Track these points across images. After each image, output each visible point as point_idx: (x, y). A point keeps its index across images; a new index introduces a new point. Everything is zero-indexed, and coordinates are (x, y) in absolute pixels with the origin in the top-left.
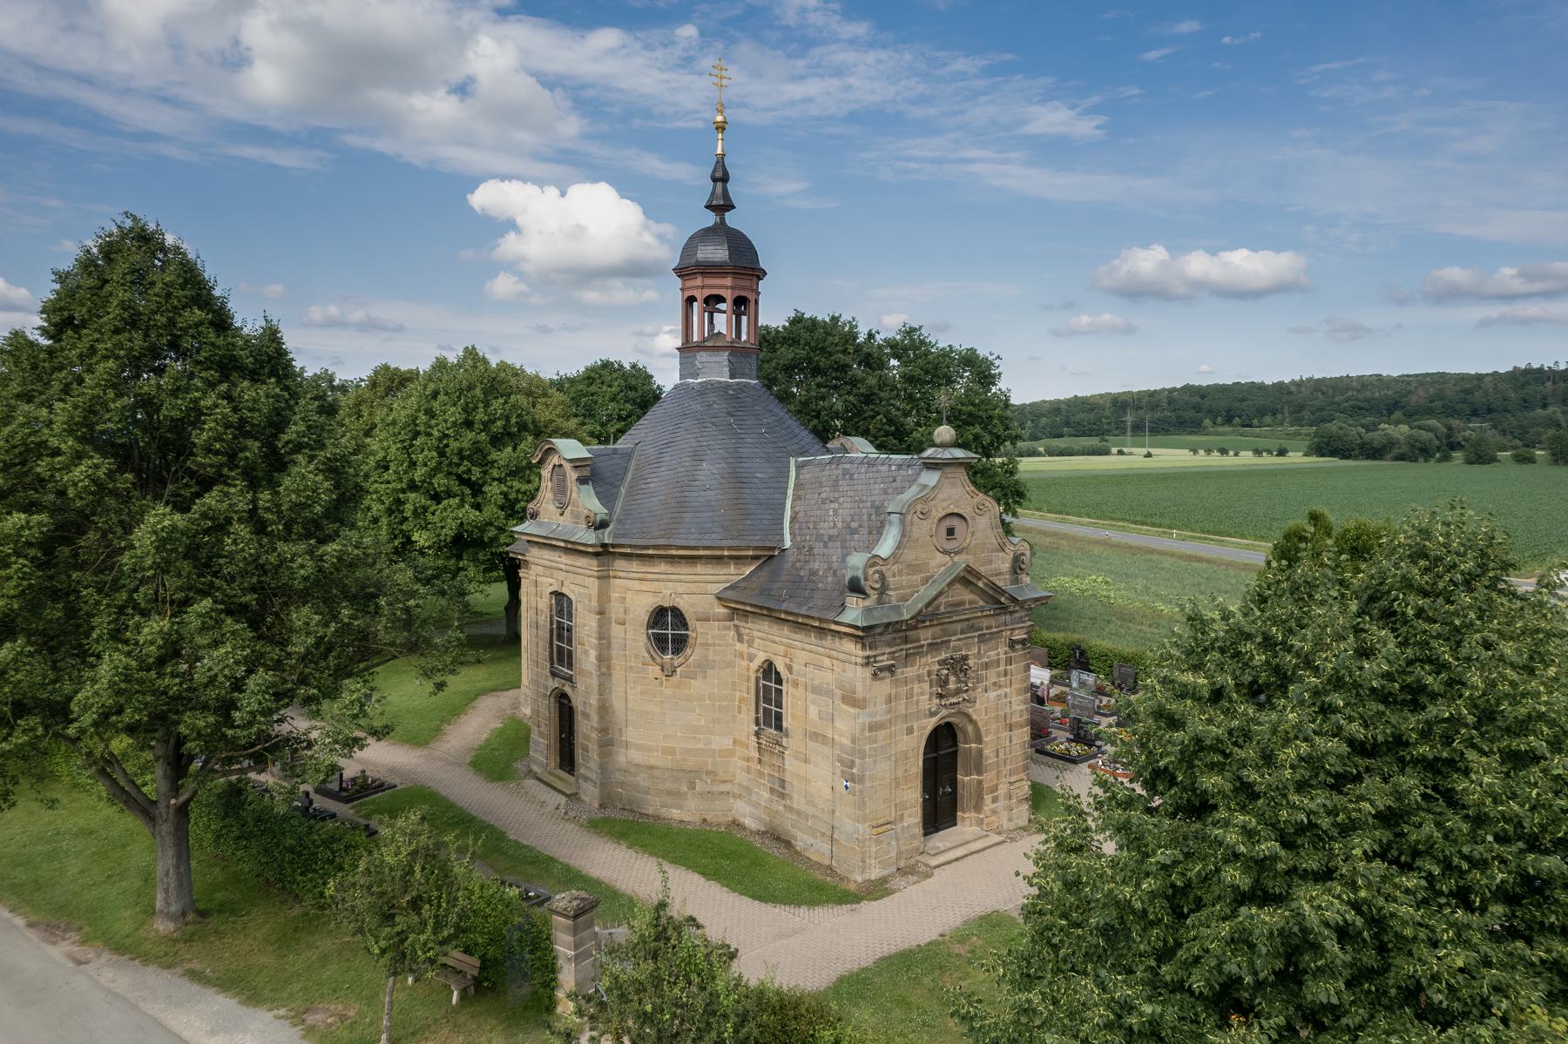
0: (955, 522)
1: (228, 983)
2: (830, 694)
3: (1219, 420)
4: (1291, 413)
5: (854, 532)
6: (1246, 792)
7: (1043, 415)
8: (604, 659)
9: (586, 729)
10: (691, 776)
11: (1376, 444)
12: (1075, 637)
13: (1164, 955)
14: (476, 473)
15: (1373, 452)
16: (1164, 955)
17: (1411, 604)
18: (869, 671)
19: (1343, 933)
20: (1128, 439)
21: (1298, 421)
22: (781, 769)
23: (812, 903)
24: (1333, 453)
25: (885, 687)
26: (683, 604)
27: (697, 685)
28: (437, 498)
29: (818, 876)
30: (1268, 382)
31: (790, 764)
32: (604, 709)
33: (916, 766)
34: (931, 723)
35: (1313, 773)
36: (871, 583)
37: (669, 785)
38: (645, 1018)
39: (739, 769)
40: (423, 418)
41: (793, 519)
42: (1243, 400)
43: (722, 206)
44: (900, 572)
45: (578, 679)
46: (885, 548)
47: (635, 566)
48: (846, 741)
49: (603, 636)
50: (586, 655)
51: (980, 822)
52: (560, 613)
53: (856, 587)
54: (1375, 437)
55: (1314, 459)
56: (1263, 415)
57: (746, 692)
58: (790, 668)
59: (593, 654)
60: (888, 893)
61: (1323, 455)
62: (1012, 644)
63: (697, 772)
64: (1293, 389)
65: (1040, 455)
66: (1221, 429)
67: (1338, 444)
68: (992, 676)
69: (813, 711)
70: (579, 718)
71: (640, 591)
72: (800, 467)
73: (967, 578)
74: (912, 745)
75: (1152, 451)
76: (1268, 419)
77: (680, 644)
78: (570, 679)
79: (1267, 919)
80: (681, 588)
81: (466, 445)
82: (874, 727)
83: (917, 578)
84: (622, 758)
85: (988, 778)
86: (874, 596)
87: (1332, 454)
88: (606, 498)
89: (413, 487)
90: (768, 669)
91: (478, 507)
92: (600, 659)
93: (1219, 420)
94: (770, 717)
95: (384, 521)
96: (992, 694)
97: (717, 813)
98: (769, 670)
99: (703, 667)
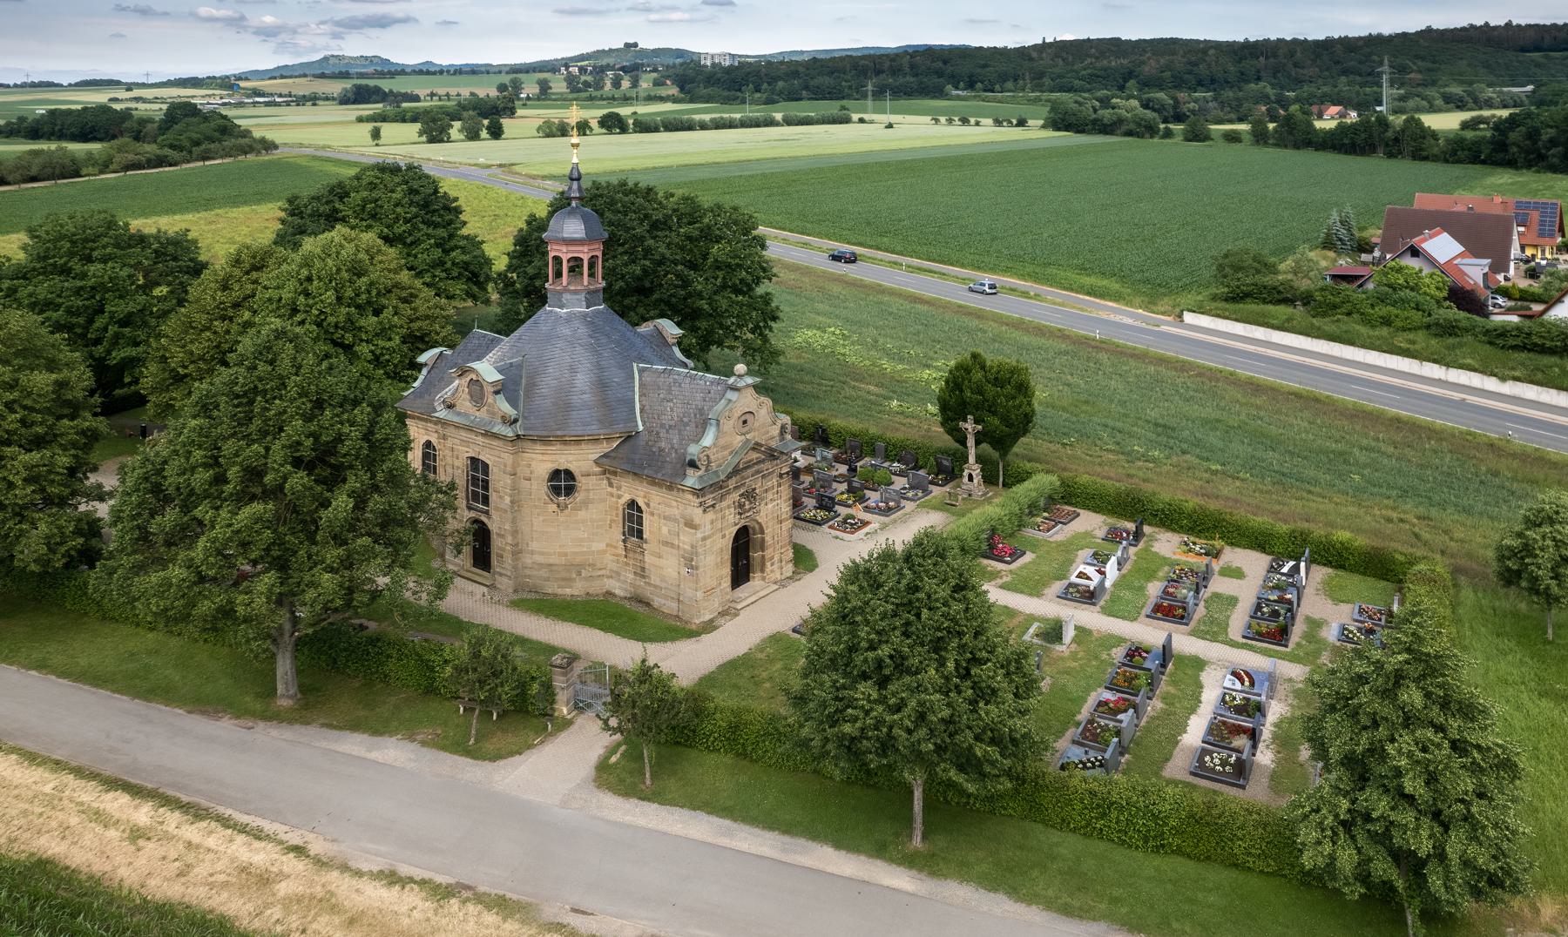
0: (748, 417)
1: (355, 726)
2: (676, 520)
4: (1032, 79)
5: (686, 425)
6: (867, 622)
7: (780, 78)
10: (579, 568)
12: (818, 417)
13: (847, 665)
14: (349, 338)
15: (1106, 129)
16: (847, 665)
17: (917, 560)
19: (891, 657)
20: (870, 103)
21: (1038, 87)
22: (642, 561)
23: (673, 640)
24: (1067, 128)
25: (710, 515)
26: (572, 468)
27: (582, 514)
30: (1011, 46)
31: (648, 558)
33: (728, 556)
35: (884, 616)
36: (702, 463)
37: (563, 575)
40: (302, 298)
41: (642, 411)
42: (985, 66)
45: (492, 512)
46: (708, 440)
47: (539, 447)
48: (688, 547)
51: (763, 579)
53: (692, 464)
54: (1106, 114)
58: (648, 505)
60: (716, 628)
61: (1059, 129)
62: (781, 476)
64: (1034, 55)
65: (777, 124)
67: (1073, 120)
68: (770, 496)
69: (665, 530)
70: (494, 537)
71: (542, 461)
72: (641, 371)
73: (756, 447)
74: (726, 543)
75: (893, 118)
76: (1009, 84)
77: (570, 490)
78: (487, 513)
79: (870, 655)
80: (571, 458)
81: (342, 319)
82: (704, 539)
84: (528, 560)
85: (768, 553)
87: (1067, 129)
88: (513, 402)
90: (632, 504)
97: (597, 588)
98: (632, 504)
99: (586, 503)
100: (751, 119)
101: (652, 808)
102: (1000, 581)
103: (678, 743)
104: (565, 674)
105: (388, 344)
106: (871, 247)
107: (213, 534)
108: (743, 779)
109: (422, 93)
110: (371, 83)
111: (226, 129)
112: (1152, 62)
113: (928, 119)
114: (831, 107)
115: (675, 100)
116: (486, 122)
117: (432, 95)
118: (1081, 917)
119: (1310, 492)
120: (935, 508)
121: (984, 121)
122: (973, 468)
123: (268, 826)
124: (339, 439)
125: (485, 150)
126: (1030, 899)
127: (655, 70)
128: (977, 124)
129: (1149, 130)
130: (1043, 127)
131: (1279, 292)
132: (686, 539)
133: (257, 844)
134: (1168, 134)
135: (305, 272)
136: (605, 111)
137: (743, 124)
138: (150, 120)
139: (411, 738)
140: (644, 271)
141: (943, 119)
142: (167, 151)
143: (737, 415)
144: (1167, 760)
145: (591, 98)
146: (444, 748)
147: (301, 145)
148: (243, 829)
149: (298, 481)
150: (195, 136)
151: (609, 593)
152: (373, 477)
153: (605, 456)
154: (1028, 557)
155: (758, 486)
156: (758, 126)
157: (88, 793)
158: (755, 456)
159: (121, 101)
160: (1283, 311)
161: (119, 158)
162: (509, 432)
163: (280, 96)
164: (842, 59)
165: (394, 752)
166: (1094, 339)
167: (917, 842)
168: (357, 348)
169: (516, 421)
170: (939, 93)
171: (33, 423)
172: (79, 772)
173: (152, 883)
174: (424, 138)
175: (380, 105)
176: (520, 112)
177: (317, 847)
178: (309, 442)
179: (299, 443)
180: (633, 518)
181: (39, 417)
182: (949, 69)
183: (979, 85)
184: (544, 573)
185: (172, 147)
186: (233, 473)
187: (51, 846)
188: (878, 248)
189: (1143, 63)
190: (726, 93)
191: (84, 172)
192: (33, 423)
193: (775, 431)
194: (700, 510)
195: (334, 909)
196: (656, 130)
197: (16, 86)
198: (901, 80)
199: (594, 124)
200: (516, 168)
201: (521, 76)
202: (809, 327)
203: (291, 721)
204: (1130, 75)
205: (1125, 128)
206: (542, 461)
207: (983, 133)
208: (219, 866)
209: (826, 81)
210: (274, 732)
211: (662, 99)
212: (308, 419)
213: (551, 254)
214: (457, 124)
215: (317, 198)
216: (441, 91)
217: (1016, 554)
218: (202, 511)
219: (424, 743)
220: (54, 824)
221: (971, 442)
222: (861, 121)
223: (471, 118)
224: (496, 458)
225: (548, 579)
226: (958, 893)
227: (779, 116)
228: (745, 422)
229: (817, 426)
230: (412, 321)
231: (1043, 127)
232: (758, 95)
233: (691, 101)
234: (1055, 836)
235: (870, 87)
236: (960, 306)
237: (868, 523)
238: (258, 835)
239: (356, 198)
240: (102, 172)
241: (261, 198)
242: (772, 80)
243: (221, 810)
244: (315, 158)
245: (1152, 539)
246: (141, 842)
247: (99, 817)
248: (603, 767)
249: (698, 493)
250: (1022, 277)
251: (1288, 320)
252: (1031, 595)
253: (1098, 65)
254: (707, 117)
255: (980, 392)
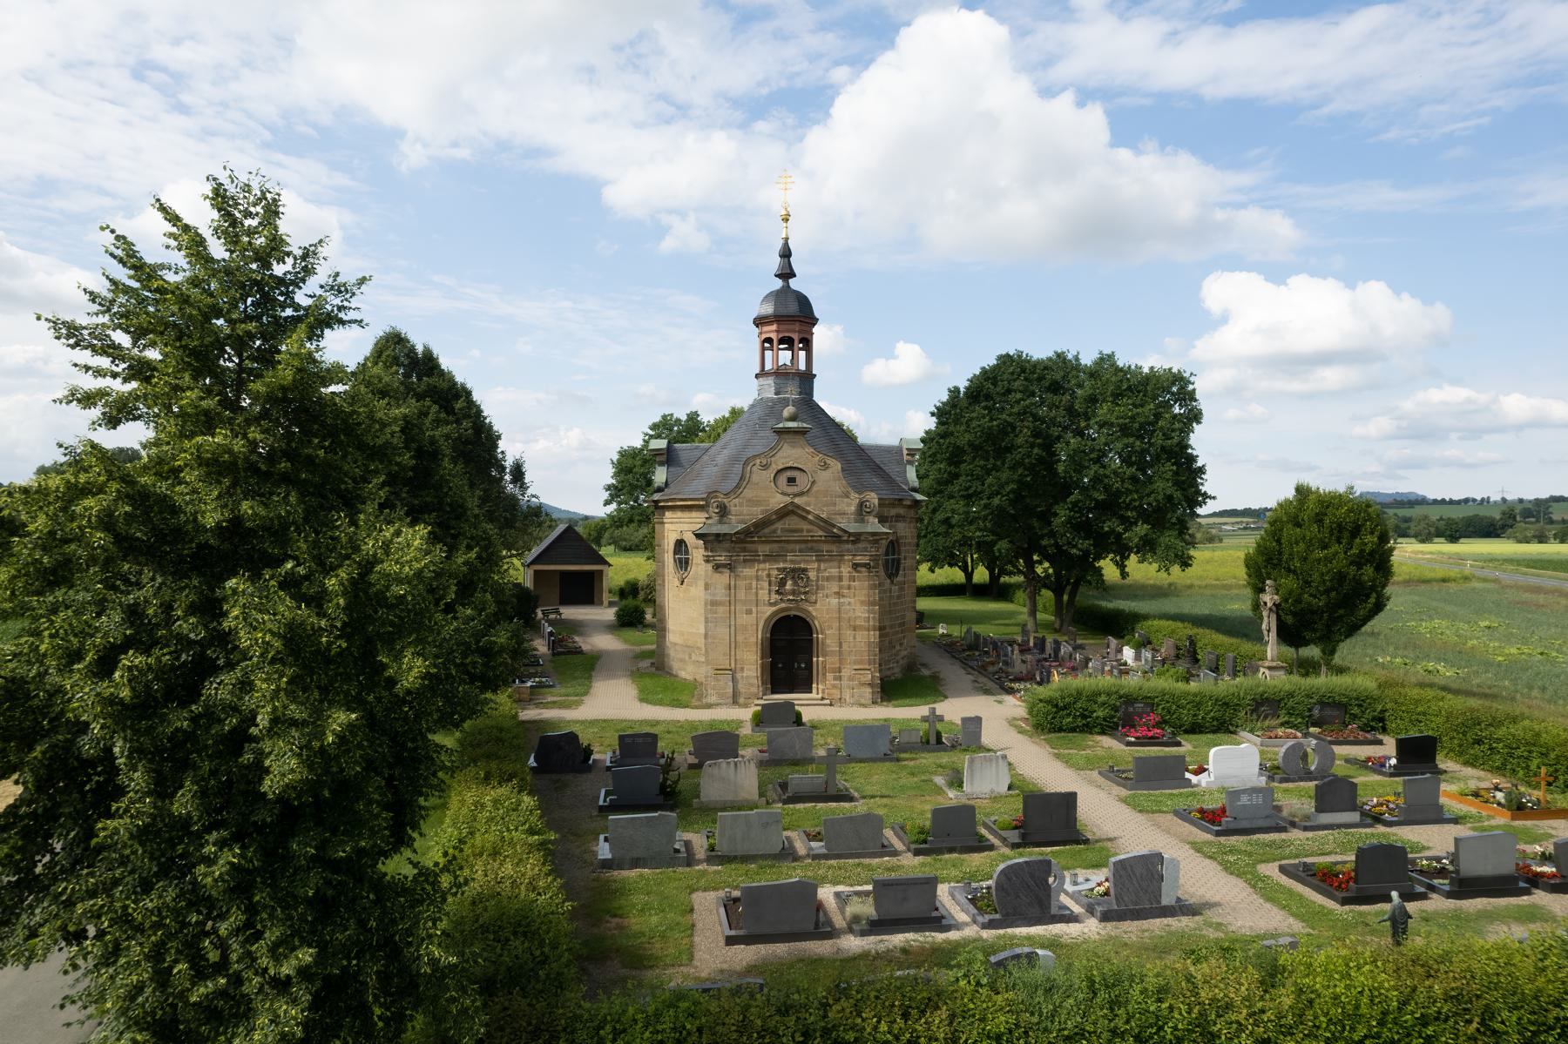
18: (710, 566)
43: (786, 274)
44: (741, 505)
62: (856, 566)
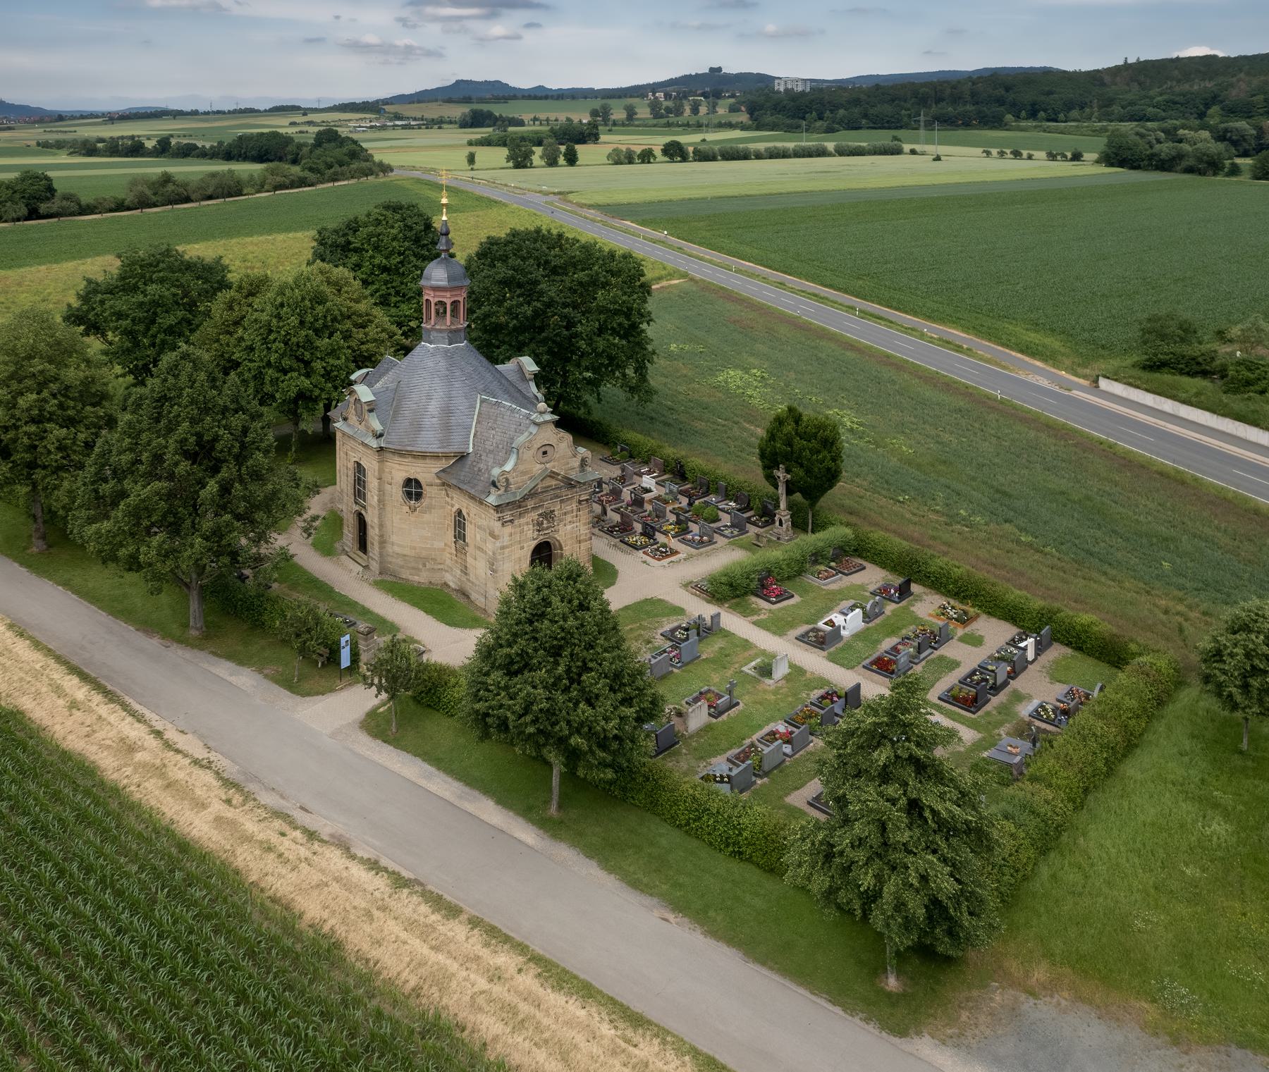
1: (230, 657)
3: (1023, 114)
4: (1100, 107)
7: (842, 106)
8: (381, 501)
9: (373, 533)
10: (424, 560)
11: (1163, 156)
14: (307, 356)
15: (1164, 165)
20: (922, 132)
24: (1122, 164)
25: (508, 529)
27: (427, 517)
28: (285, 372)
29: (478, 614)
31: (469, 560)
32: (381, 526)
34: (534, 544)
36: (502, 483)
38: (388, 671)
39: (448, 556)
40: (274, 321)
42: (1050, 93)
45: (368, 508)
46: (508, 467)
49: (381, 490)
50: (372, 497)
52: (359, 472)
55: (1103, 169)
56: (1070, 109)
57: (450, 522)
59: (376, 498)
61: (1112, 165)
62: (580, 502)
63: (426, 559)
64: (1107, 79)
65: (830, 155)
66: (1023, 124)
67: (1127, 154)
68: (569, 518)
70: (369, 527)
71: (399, 471)
72: (483, 401)
73: (553, 475)
75: (942, 150)
76: (1075, 113)
77: (419, 496)
78: (364, 507)
80: (419, 470)
82: (503, 548)
83: (526, 477)
86: (503, 489)
89: (269, 364)
91: (308, 376)
92: (379, 501)
93: (1023, 114)
94: (460, 536)
95: (252, 384)
96: (569, 527)
97: (437, 579)
98: (460, 513)
99: (430, 508)
100: (803, 149)
101: (388, 749)
102: (755, 618)
103: (429, 706)
104: (366, 640)
105: (338, 362)
106: (839, 289)
107: (128, 500)
108: (462, 741)
109: (527, 117)
110: (485, 107)
111: (356, 153)
112: (1243, 86)
113: (979, 151)
114: (883, 137)
115: (744, 128)
116: (563, 148)
117: (535, 119)
118: (642, 891)
119: (1105, 573)
120: (742, 547)
121: (1036, 154)
122: (783, 513)
123: (148, 714)
124: (216, 439)
125: (562, 175)
126: (610, 870)
127: (733, 96)
128: (1030, 157)
129: (1211, 166)
130: (1097, 162)
131: (1198, 363)
132: (490, 546)
133: (137, 725)
134: (1235, 171)
135: (279, 300)
136: (668, 139)
137: (798, 154)
138: (305, 145)
139: (260, 672)
140: (536, 311)
141: (994, 152)
142: (307, 174)
143: (536, 446)
144: (797, 788)
145: (668, 125)
146: (276, 682)
147: (414, 168)
148: (133, 714)
149: (184, 467)
150: (329, 159)
151: (446, 584)
152: (239, 470)
153: (443, 471)
154: (796, 599)
155: (557, 509)
156: (810, 156)
157: (58, 674)
158: (554, 482)
159: (283, 126)
160: (1199, 383)
161: (271, 180)
162: (374, 443)
163: (415, 119)
164: (903, 86)
165: (245, 679)
166: (995, 400)
167: (553, 810)
168: (313, 364)
169: (381, 435)
170: (995, 122)
171: (68, 408)
172: (60, 659)
173: (70, 737)
174: (511, 164)
175: (490, 129)
176: (603, 138)
177: (171, 735)
178: (192, 439)
179: (186, 440)
180: (460, 521)
181: (72, 403)
182: (1011, 96)
183: (1042, 114)
184: (400, 561)
185: (311, 169)
186: (145, 456)
187: (26, 703)
188: (846, 292)
189: (1232, 85)
190: (788, 121)
191: (245, 191)
192: (68, 408)
193: (576, 463)
194: (499, 524)
195: (163, 775)
196: (714, 159)
197: (229, 112)
198: (961, 109)
199: (658, 151)
200: (571, 197)
201: (610, 102)
202: (736, 367)
203: (193, 646)
204: (1214, 99)
205: (1185, 164)
206: (399, 471)
207: (1036, 167)
208: (110, 735)
209: (887, 109)
210: (180, 652)
211: (731, 126)
212: (193, 421)
213: (425, 297)
214: (538, 150)
215: (336, 231)
216: (543, 116)
217: (782, 597)
218: (127, 484)
219: (266, 676)
220: (33, 690)
221: (782, 490)
222: (913, 152)
223: (550, 145)
224: (371, 464)
225: (402, 567)
226: (564, 853)
227: (830, 146)
228: (545, 453)
229: (678, 462)
230: (363, 343)
231: (1097, 162)
232: (819, 123)
233: (758, 128)
234: (665, 829)
235: (922, 118)
236: (888, 356)
237: (677, 552)
238: (140, 719)
239: (363, 232)
240: (259, 191)
241: (302, 228)
242: (835, 107)
243: (128, 700)
244: (419, 181)
245: (919, 598)
246: (74, 711)
247: (58, 690)
248: (372, 714)
249: (498, 508)
250: (966, 329)
251: (1198, 394)
252: (774, 633)
253: (1177, 89)
254: (761, 146)
255: (790, 444)
